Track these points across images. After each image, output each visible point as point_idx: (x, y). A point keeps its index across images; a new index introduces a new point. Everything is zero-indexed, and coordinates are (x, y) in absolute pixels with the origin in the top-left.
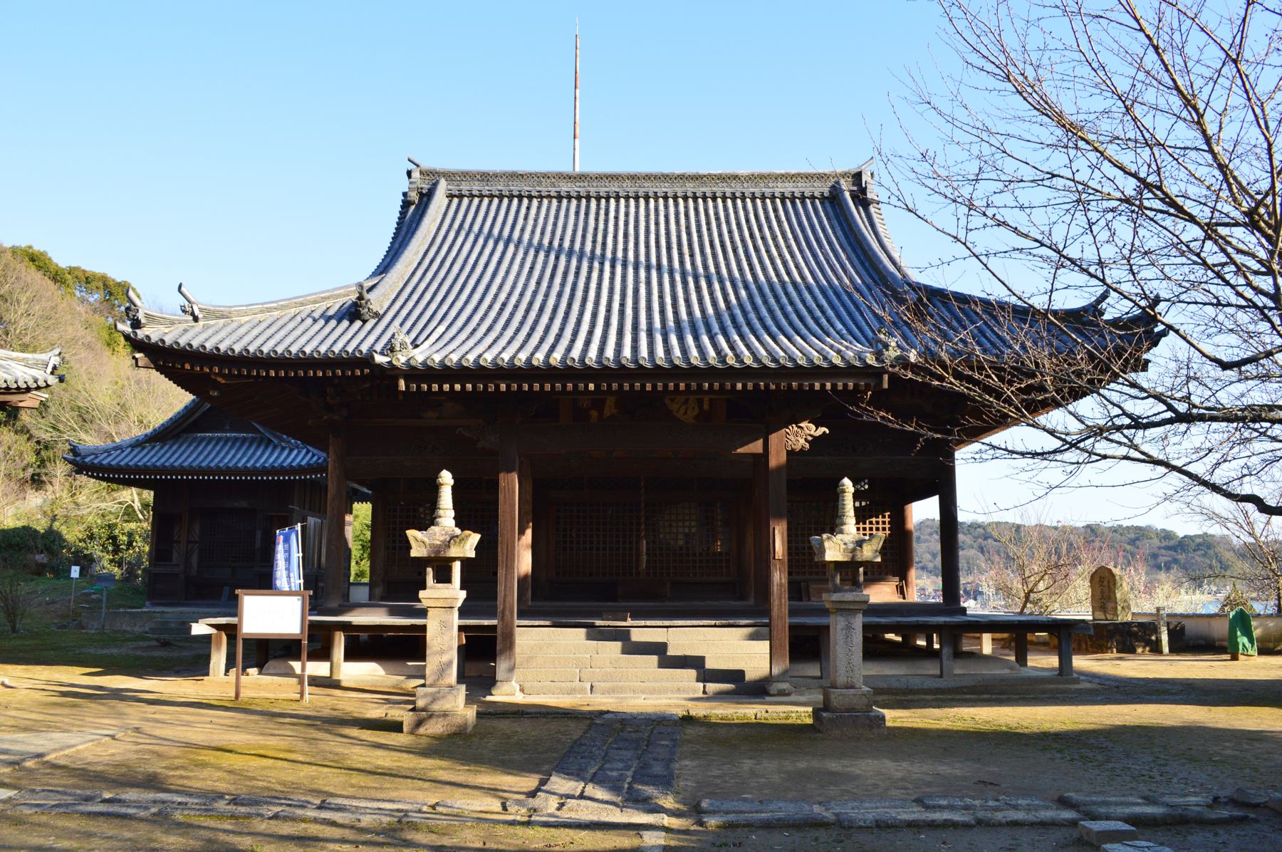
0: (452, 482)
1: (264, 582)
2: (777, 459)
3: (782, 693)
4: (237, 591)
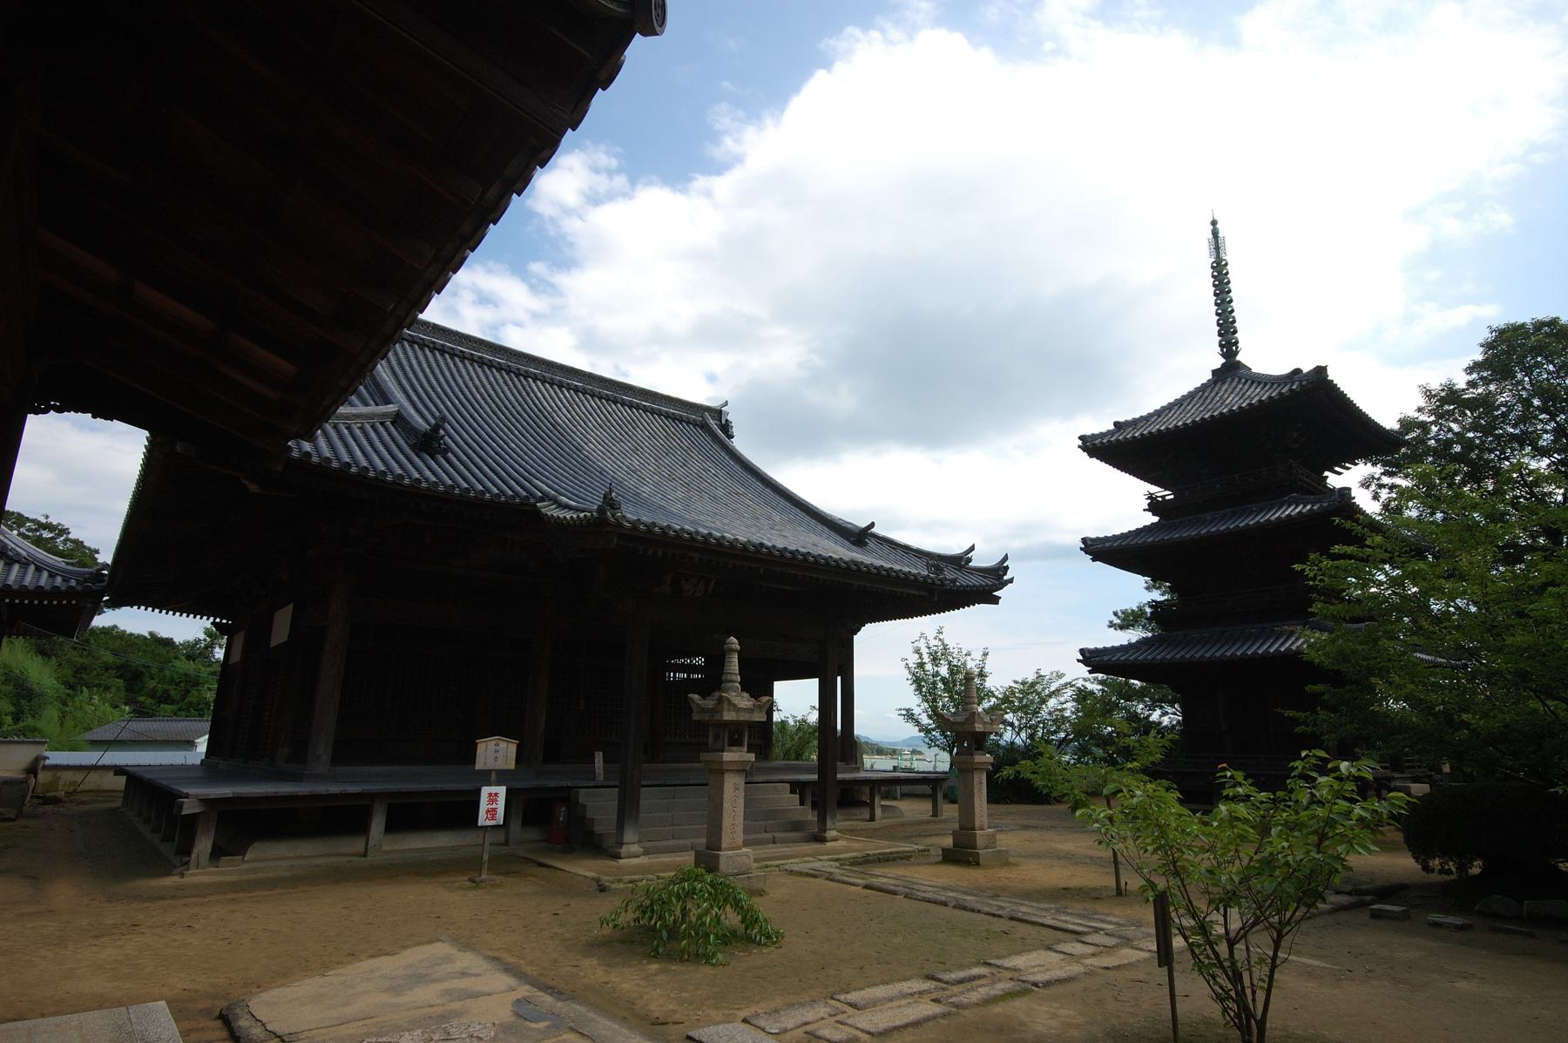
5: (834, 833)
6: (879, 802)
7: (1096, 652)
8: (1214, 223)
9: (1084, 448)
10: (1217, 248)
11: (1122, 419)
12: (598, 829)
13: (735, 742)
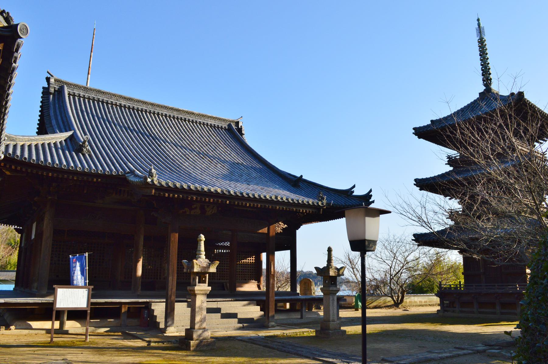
0: (204, 239)
1: (68, 282)
2: (272, 233)
3: (273, 326)
4: (54, 286)
5: (273, 323)
6: (305, 310)
8: (478, 20)
9: (415, 134)
10: (480, 32)
11: (434, 119)
12: (158, 320)
13: (201, 281)
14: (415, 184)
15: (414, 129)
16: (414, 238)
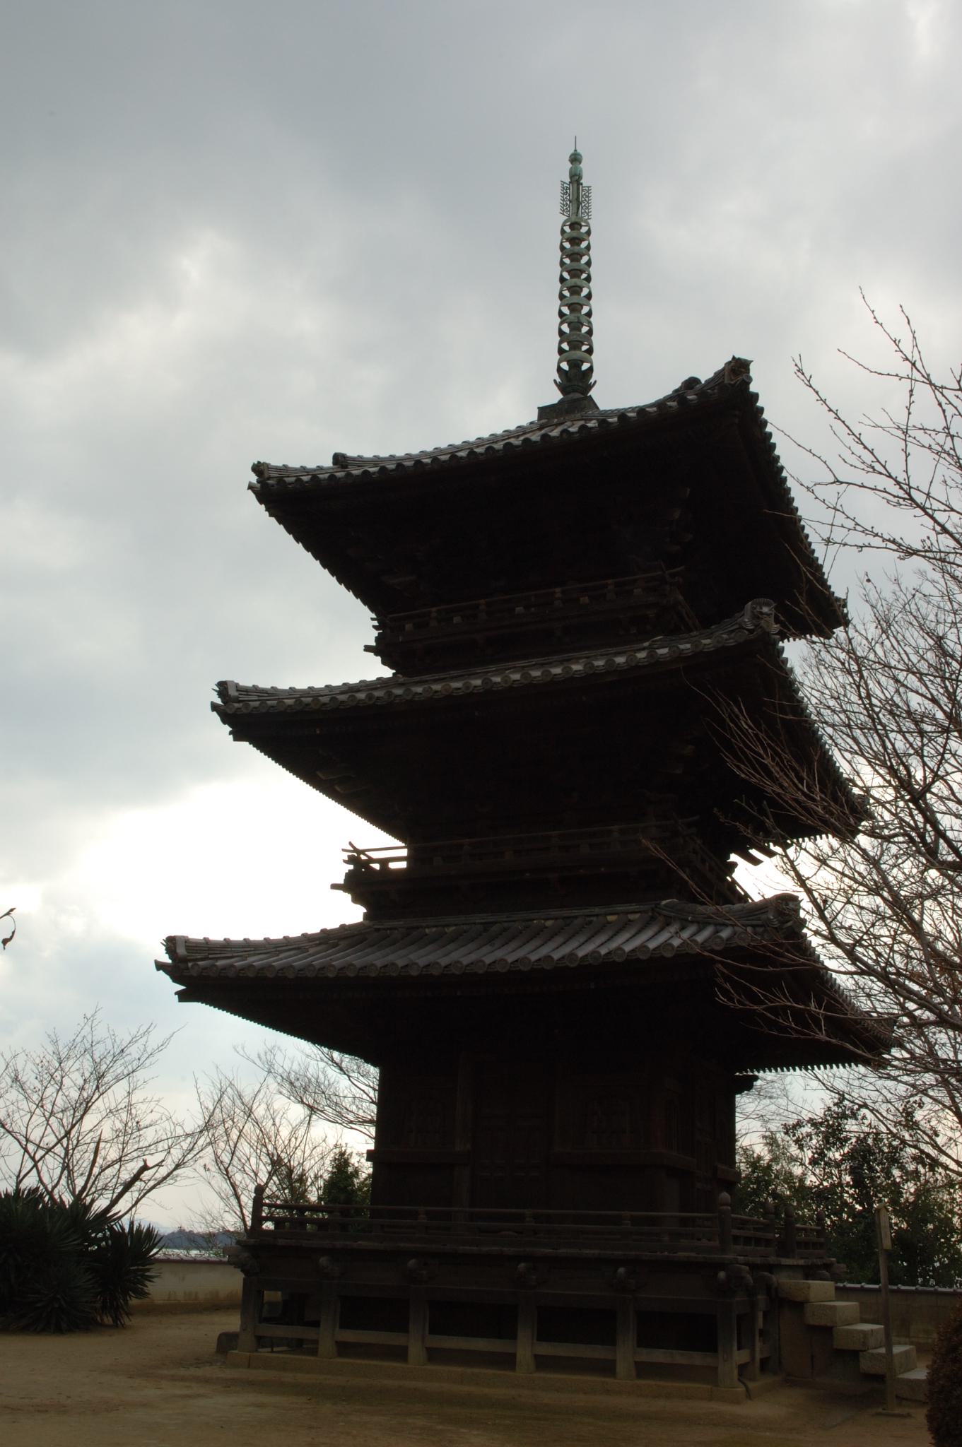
7: (206, 948)
8: (575, 159)
9: (181, 1000)
11: (351, 452)
14: (214, 707)
15: (258, 469)
16: (166, 959)
